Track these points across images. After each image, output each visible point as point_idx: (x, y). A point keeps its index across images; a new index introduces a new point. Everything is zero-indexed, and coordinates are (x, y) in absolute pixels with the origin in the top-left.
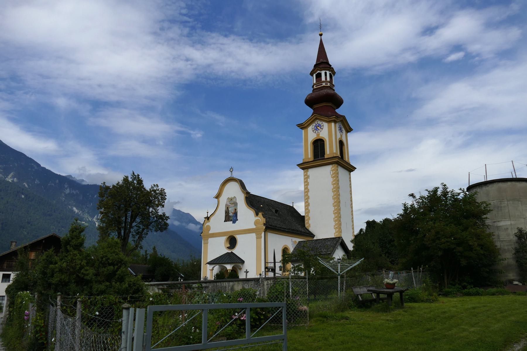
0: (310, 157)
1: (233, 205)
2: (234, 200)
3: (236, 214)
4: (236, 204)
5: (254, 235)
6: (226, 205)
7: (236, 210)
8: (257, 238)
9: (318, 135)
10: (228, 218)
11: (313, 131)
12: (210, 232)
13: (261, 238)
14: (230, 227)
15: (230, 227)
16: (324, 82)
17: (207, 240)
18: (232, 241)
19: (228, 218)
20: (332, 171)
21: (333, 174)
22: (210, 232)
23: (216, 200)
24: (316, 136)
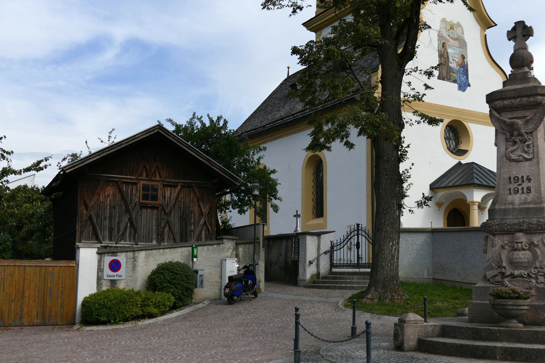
2: (459, 31)
3: (464, 68)
7: (463, 57)
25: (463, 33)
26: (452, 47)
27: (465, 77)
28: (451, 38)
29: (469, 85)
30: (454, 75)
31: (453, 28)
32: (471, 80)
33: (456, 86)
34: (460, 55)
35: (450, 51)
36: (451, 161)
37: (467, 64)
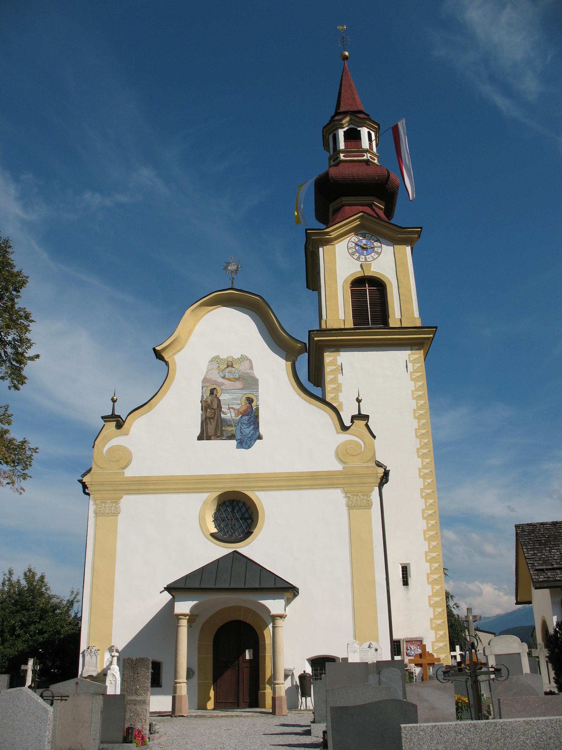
0: (342, 317)
1: (239, 384)
2: (243, 368)
3: (251, 415)
4: (250, 382)
5: (337, 496)
6: (205, 380)
7: (250, 401)
8: (350, 507)
10: (213, 425)
11: (352, 255)
12: (129, 472)
13: (369, 505)
14: (225, 460)
15: (225, 460)
16: (366, 151)
17: (116, 501)
18: (236, 514)
19: (213, 425)
20: (413, 362)
22: (129, 472)
25: (251, 368)
26: (226, 391)
27: (252, 427)
28: (229, 379)
29: (260, 438)
30: (230, 429)
31: (232, 366)
32: (262, 430)
33: (234, 443)
34: (244, 398)
35: (224, 397)
36: (221, 551)
37: (257, 409)
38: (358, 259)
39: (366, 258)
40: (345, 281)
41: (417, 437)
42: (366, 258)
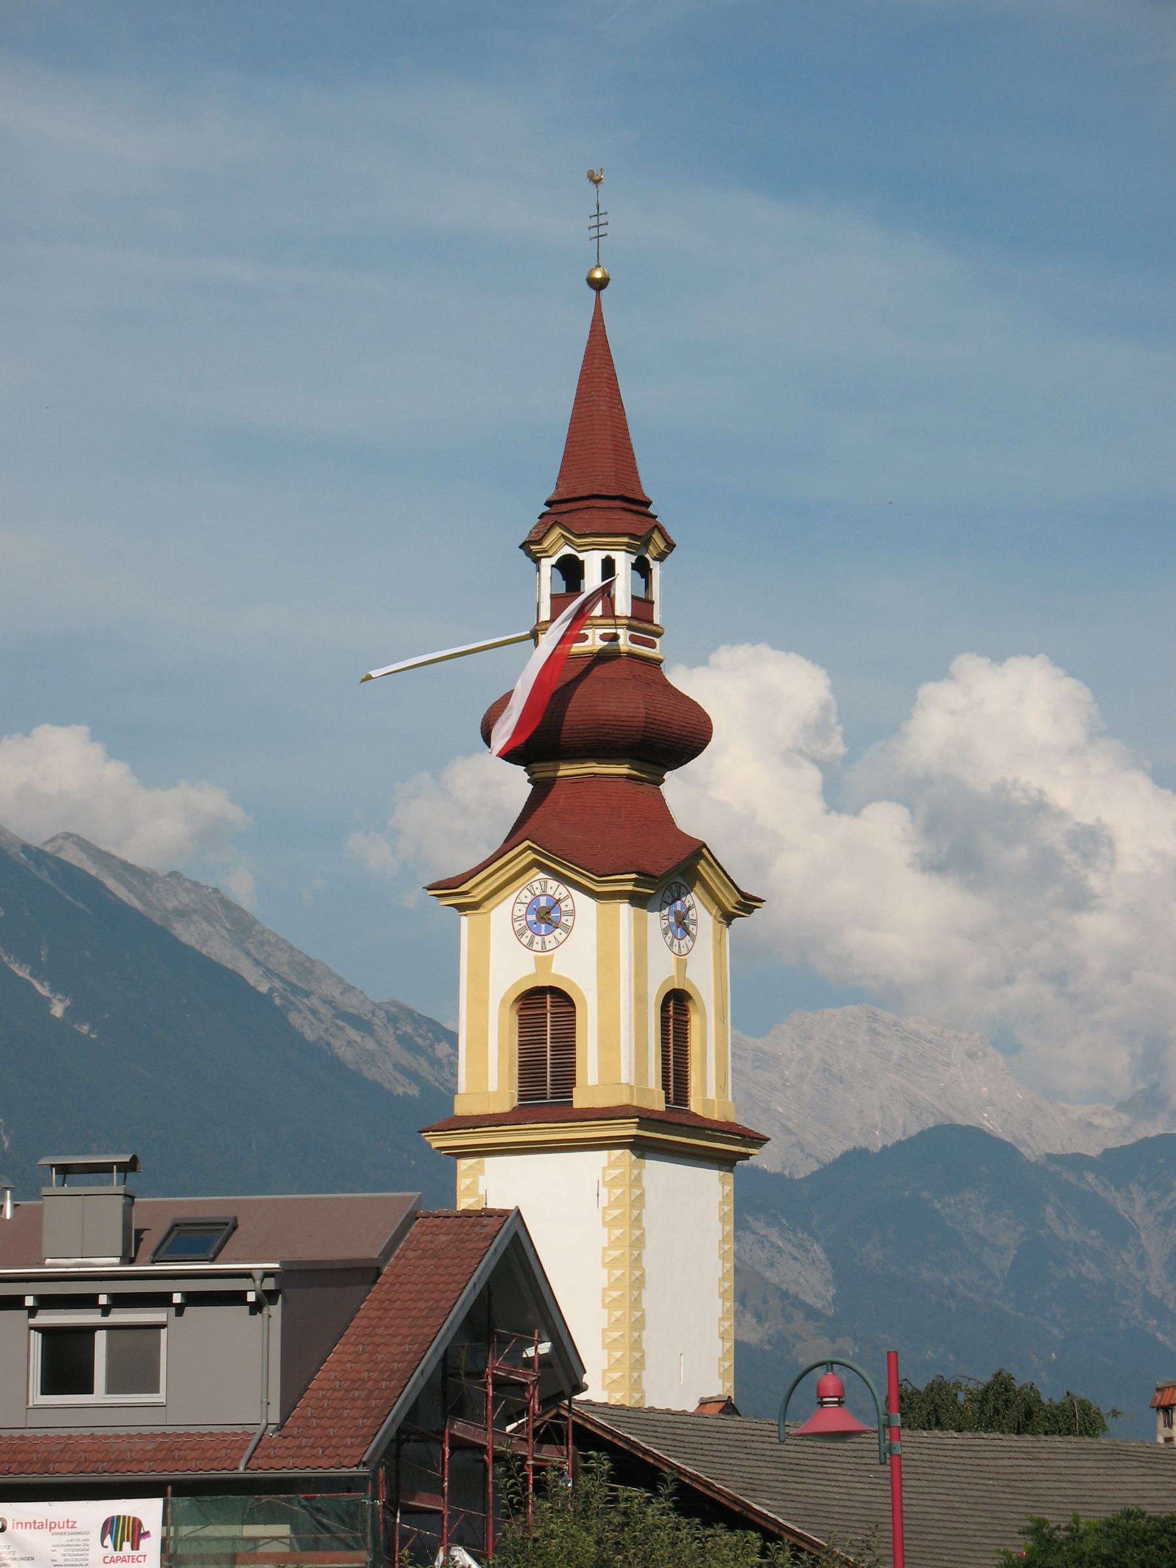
0: (493, 1085)
9: (543, 964)
21: (611, 1206)
23: (594, 292)
24: (532, 970)
38: (529, 946)
39: (543, 942)
40: (503, 1001)
41: (604, 1346)
42: (543, 942)
